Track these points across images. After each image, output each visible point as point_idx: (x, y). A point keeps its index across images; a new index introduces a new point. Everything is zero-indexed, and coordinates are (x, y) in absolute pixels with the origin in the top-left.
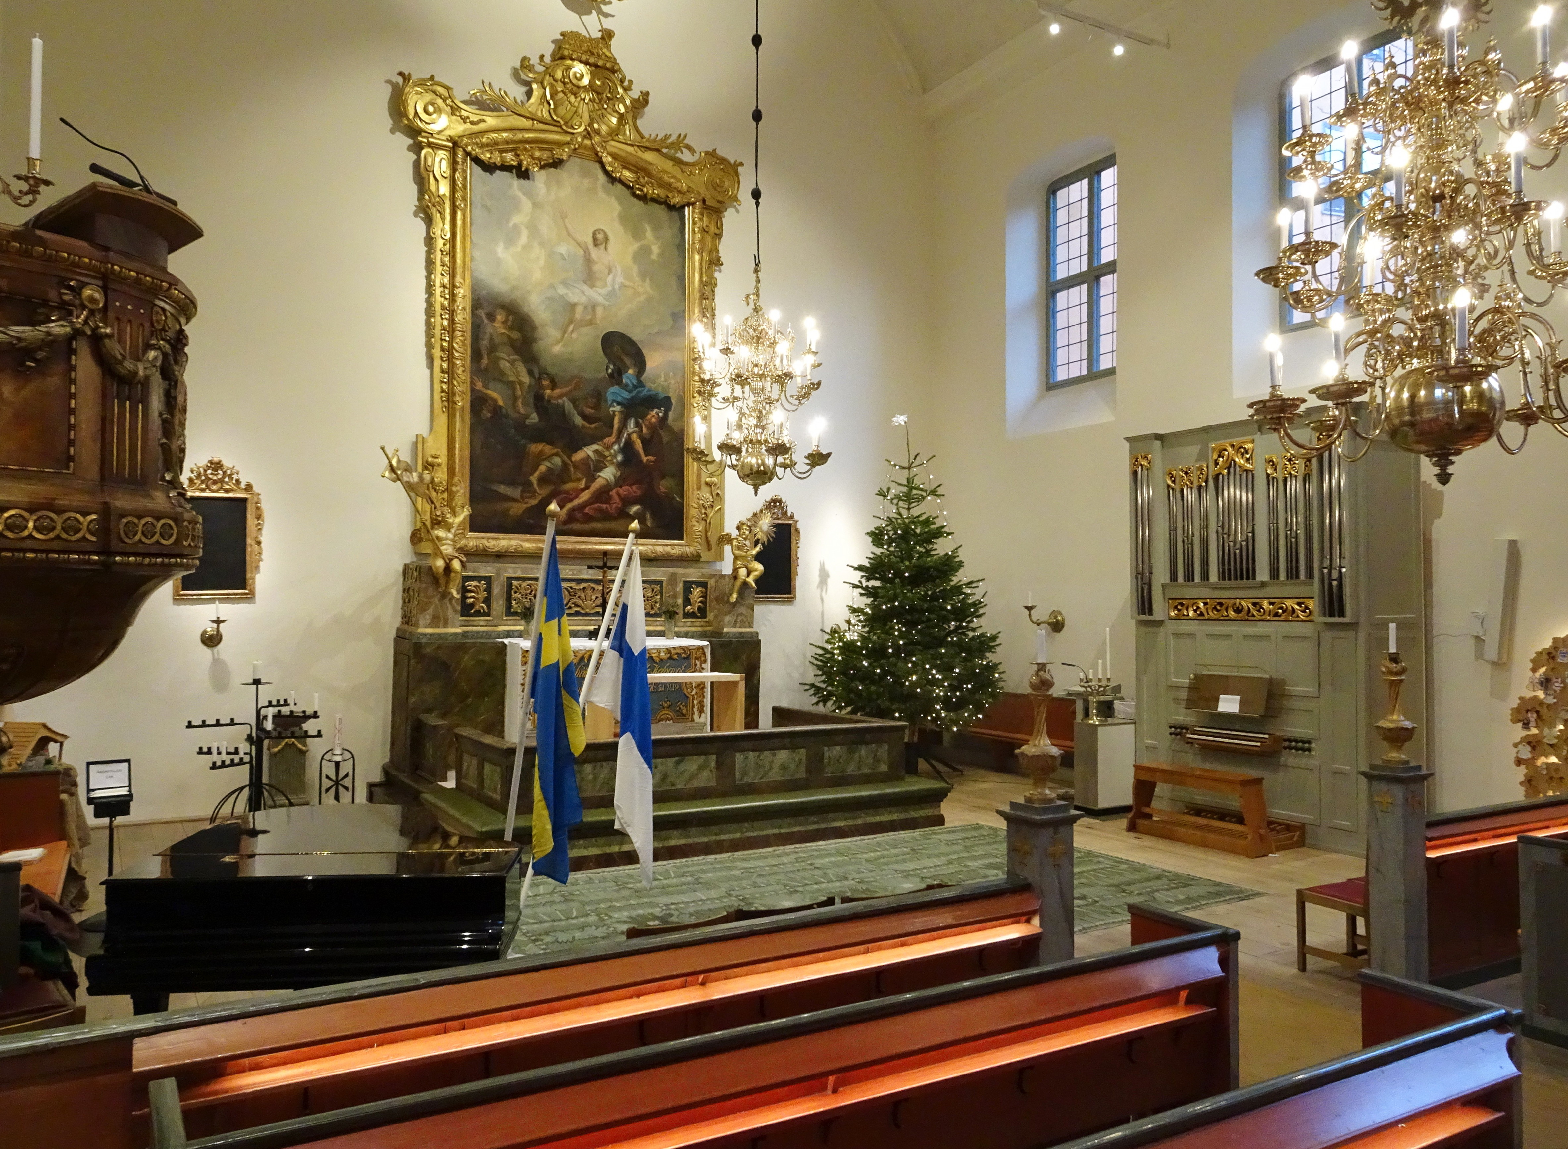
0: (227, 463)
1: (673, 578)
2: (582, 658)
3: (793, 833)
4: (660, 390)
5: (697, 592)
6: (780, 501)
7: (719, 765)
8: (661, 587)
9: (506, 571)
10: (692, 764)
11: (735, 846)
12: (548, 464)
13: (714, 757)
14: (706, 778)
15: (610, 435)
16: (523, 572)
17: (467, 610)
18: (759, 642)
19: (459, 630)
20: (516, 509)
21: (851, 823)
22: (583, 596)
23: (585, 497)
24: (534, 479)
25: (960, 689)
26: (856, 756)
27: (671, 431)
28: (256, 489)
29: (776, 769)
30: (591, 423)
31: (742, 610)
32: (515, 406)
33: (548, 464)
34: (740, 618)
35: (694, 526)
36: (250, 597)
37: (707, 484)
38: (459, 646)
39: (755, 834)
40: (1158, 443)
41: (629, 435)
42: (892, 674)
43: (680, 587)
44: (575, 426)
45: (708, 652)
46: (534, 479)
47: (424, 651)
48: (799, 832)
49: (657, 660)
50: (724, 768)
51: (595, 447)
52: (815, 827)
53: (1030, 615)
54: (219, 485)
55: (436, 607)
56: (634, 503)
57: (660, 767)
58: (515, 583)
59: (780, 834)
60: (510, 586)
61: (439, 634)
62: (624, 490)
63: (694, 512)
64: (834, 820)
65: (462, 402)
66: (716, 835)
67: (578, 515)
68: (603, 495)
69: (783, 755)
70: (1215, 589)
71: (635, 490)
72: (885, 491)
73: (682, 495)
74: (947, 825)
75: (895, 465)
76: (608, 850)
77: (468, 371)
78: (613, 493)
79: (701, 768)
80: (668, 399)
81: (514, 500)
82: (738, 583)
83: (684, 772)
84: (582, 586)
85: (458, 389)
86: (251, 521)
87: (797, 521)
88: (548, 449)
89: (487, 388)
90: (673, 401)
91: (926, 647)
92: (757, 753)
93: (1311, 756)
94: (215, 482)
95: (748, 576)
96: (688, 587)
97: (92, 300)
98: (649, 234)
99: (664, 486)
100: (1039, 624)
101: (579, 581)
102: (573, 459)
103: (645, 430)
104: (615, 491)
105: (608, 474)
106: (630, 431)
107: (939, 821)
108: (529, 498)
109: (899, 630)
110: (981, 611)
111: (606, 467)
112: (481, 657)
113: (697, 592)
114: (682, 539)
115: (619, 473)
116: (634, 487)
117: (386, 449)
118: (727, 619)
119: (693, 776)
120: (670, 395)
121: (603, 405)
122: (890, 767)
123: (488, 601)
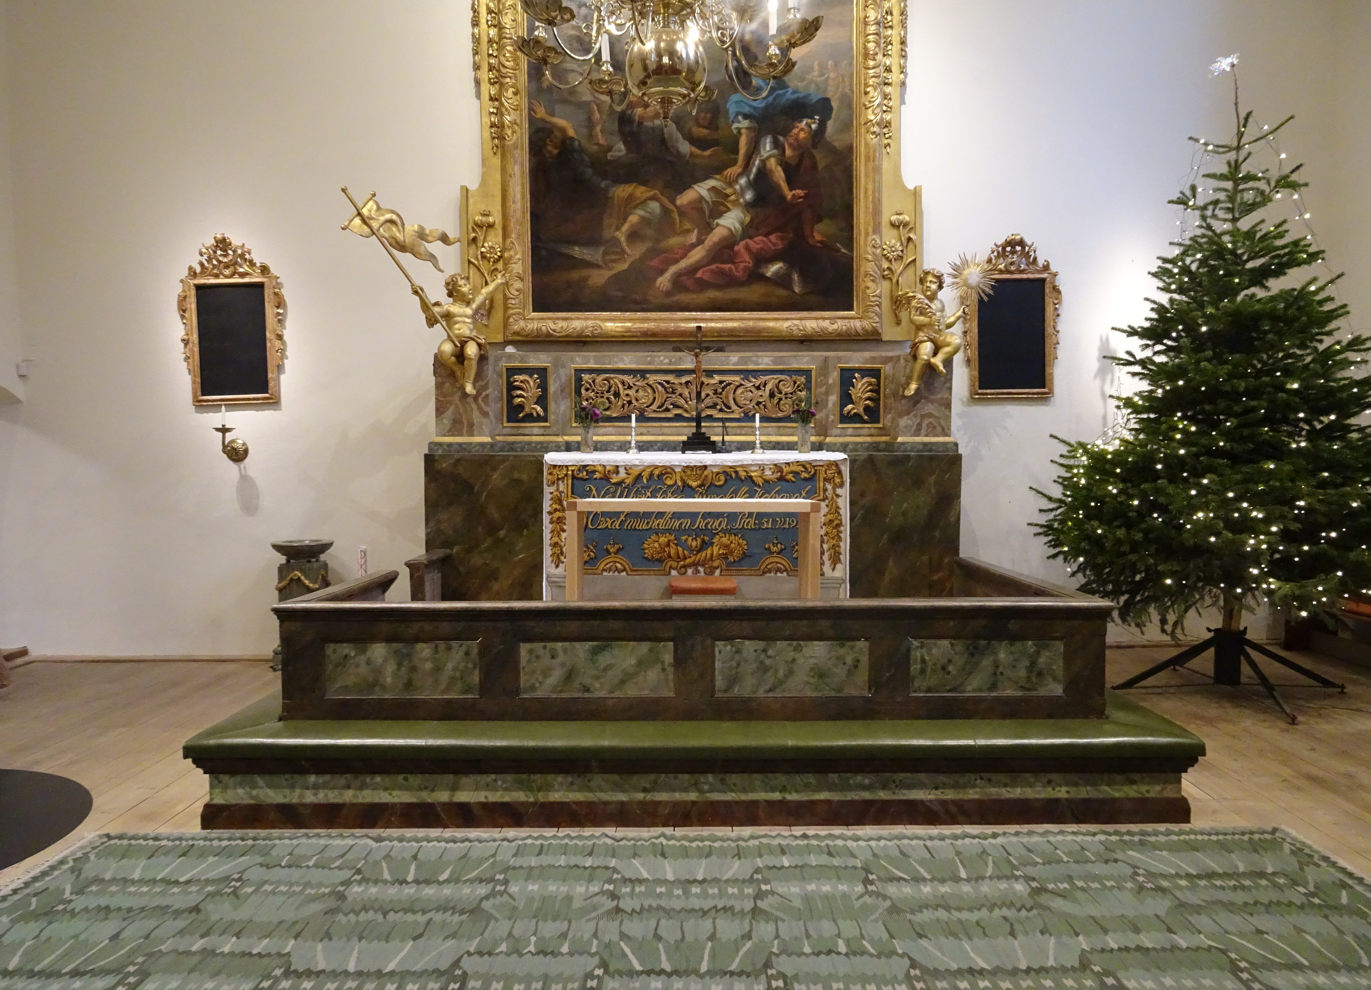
0: (236, 241)
1: (825, 367)
2: (639, 477)
3: (813, 802)
4: (812, 89)
5: (861, 387)
6: (1021, 243)
7: (679, 662)
8: (809, 380)
9: (573, 361)
10: (625, 656)
11: (683, 816)
12: (641, 213)
15: (734, 163)
18: (958, 458)
19: (487, 439)
20: (598, 278)
21: (950, 795)
23: (697, 255)
24: (621, 235)
25: (1313, 539)
26: (987, 662)
27: (832, 150)
28: (274, 270)
29: (801, 677)
30: (704, 148)
31: (929, 408)
32: (591, 136)
33: (641, 213)
34: (926, 422)
35: (871, 288)
36: (274, 402)
37: (893, 225)
41: (763, 162)
42: (1163, 510)
43: (834, 377)
44: (679, 155)
47: (438, 466)
48: (828, 802)
49: (760, 481)
51: (711, 183)
52: (867, 795)
54: (232, 269)
55: (457, 406)
57: (561, 658)
58: (586, 377)
59: (783, 802)
60: (579, 381)
61: (460, 445)
62: (757, 243)
63: (870, 267)
64: (910, 787)
65: (519, 137)
66: (645, 790)
67: (689, 282)
69: (818, 651)
71: (775, 241)
72: (1188, 193)
73: (849, 242)
74: (1197, 822)
75: (1206, 144)
76: (427, 797)
77: (523, 93)
79: (642, 664)
80: (826, 102)
81: (597, 266)
82: (918, 366)
84: (684, 380)
85: (507, 119)
86: (270, 311)
87: (1055, 275)
88: (641, 191)
89: (553, 115)
90: (834, 104)
91: (1234, 458)
92: (761, 644)
94: (227, 267)
95: (935, 354)
99: (820, 232)
101: (680, 373)
102: (678, 202)
103: (788, 152)
104: (742, 244)
105: (732, 220)
106: (765, 155)
107: (1179, 811)
108: (614, 261)
109: (1185, 431)
111: (729, 210)
112: (516, 475)
113: (861, 387)
114: (850, 308)
115: (748, 219)
116: (773, 237)
117: (350, 191)
118: (904, 422)
120: (829, 95)
121: (722, 121)
123: (542, 400)
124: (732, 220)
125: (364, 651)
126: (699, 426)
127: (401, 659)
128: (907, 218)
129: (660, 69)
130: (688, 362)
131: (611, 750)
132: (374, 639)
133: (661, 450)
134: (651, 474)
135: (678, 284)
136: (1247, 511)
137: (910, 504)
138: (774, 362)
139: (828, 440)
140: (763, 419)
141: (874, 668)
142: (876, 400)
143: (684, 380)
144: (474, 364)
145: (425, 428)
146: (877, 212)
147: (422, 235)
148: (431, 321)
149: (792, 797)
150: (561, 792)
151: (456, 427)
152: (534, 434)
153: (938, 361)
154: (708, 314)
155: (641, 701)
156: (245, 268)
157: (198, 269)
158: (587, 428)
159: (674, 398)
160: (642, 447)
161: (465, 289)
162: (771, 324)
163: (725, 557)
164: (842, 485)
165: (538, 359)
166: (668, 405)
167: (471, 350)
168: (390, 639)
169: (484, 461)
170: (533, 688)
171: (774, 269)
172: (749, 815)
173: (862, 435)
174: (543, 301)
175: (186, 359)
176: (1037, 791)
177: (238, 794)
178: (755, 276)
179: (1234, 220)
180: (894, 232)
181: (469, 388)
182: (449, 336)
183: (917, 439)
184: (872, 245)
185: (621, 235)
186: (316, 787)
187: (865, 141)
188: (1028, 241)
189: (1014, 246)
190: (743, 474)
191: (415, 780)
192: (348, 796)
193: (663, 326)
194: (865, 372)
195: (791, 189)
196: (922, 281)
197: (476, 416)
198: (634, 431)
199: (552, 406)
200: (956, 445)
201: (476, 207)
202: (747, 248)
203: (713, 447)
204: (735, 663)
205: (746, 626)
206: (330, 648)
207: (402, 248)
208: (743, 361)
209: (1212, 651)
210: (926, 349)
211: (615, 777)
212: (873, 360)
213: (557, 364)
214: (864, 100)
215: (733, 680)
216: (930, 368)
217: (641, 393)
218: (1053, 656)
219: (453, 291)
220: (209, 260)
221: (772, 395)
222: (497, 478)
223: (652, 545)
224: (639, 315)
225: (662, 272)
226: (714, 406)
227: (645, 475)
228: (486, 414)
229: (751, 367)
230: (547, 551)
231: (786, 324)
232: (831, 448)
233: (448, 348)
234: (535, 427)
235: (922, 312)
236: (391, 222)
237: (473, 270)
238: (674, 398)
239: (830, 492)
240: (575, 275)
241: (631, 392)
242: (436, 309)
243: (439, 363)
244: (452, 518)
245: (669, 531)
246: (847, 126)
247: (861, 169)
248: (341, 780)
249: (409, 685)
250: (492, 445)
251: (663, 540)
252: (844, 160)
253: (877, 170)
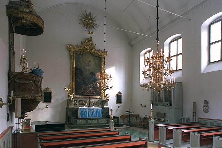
5: (101, 102)
10: (94, 120)
14: (96, 122)
17: (75, 104)
20: (80, 93)
38: (73, 108)
43: (99, 101)
46: (82, 89)
62: (93, 90)
68: (90, 91)
79: (95, 121)
98: (96, 61)
105: (91, 88)
130: (89, 100)
132: (80, 120)
135: (87, 94)
171: (94, 93)
209: (220, 43)
215: (100, 122)
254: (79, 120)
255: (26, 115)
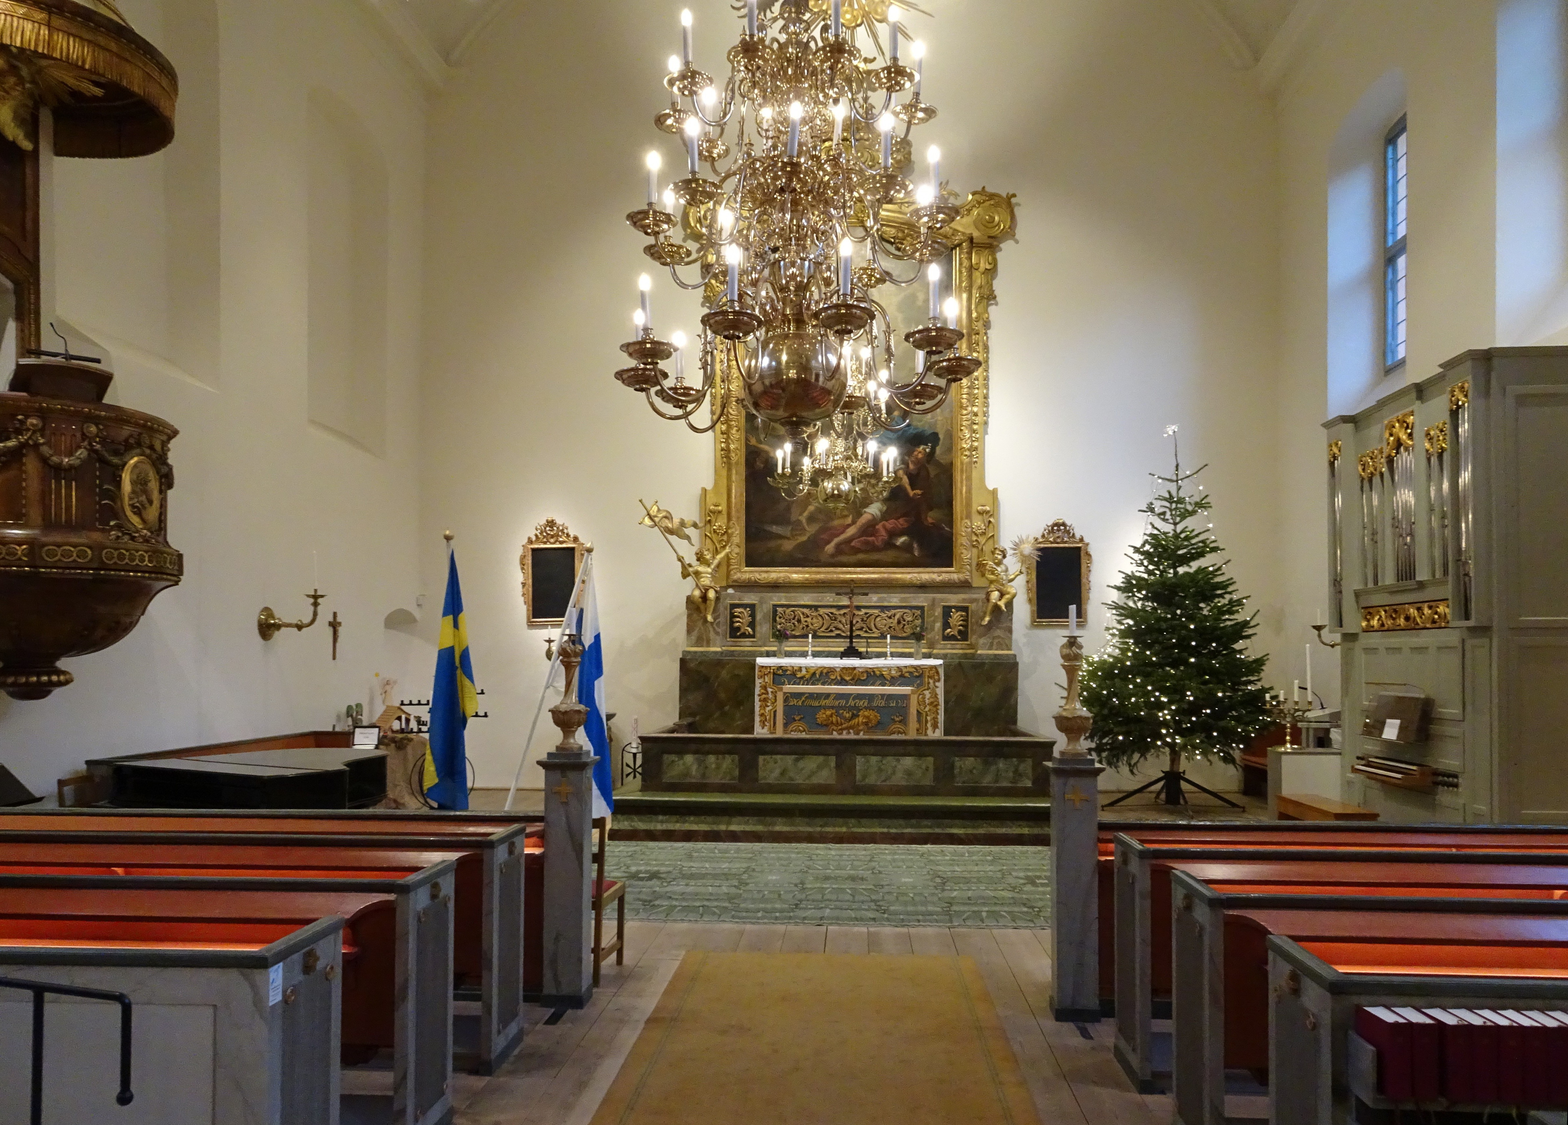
0: (559, 521)
1: (933, 603)
2: (814, 674)
6: (1064, 524)
7: (838, 766)
10: (811, 763)
11: (840, 839)
13: (834, 758)
16: (787, 599)
17: (735, 632)
19: (719, 649)
20: (788, 546)
21: (970, 831)
22: (844, 620)
23: (851, 531)
24: (803, 519)
25: (1198, 714)
26: (993, 768)
27: (938, 464)
29: (899, 774)
31: (998, 632)
34: (996, 641)
35: (964, 553)
39: (862, 830)
40: (1350, 426)
43: (938, 612)
45: (941, 671)
49: (888, 678)
50: (844, 769)
53: (1319, 636)
56: (901, 534)
59: (889, 833)
60: (775, 612)
62: (890, 524)
65: (738, 456)
68: (870, 528)
70: (1392, 593)
71: (902, 523)
73: (950, 523)
76: (715, 828)
78: (879, 527)
79: (820, 767)
83: (802, 769)
84: (842, 612)
85: (732, 447)
87: (1087, 544)
90: (941, 436)
93: (1457, 794)
94: (552, 537)
96: (947, 611)
97: (33, 425)
100: (1333, 646)
101: (839, 607)
103: (911, 466)
105: (874, 509)
110: (1250, 631)
112: (736, 672)
113: (956, 618)
114: (951, 566)
116: (901, 520)
118: (982, 641)
119: (813, 773)
122: (1033, 783)
123: (752, 625)
124: (874, 509)
125: (682, 758)
126: (851, 642)
127: (700, 763)
128: (988, 508)
129: (833, 495)
130: (845, 602)
131: (806, 804)
132: (687, 752)
133: (827, 656)
134: (821, 673)
136: (1159, 697)
137: (984, 691)
138: (902, 600)
139: (935, 651)
140: (892, 638)
141: (936, 769)
142: (966, 626)
143: (842, 612)
144: (713, 603)
145: (679, 640)
146: (969, 504)
147: (683, 524)
148: (685, 575)
149: (893, 831)
150: (780, 827)
151: (699, 642)
152: (746, 646)
153: (1002, 604)
154: (859, 569)
155: (820, 785)
156: (563, 538)
157: (534, 538)
158: (780, 642)
159: (836, 624)
160: (816, 655)
161: (708, 557)
162: (899, 576)
163: (866, 724)
164: (939, 680)
165: (750, 598)
166: (832, 628)
167: (711, 594)
168: (695, 752)
169: (717, 662)
170: (765, 778)
172: (872, 839)
173: (956, 649)
174: (751, 560)
175: (524, 595)
176: (1015, 830)
177: (625, 825)
178: (889, 545)
179: (1175, 524)
180: (980, 517)
181: (710, 618)
182: (697, 585)
183: (991, 652)
184: (965, 528)
185: (803, 519)
186: (662, 822)
187: (961, 460)
188: (1068, 523)
189: (1059, 527)
190: (878, 673)
191: (709, 819)
192: (678, 826)
193: (829, 576)
194: (959, 609)
195: (913, 489)
196: (993, 553)
197: (712, 635)
198: (810, 644)
199: (758, 628)
200: (1015, 656)
201: (711, 499)
202: (884, 526)
203: (860, 656)
204: (866, 767)
205: (872, 749)
206: (665, 756)
207: (671, 532)
208: (880, 600)
210: (995, 595)
211: (806, 820)
212: (964, 600)
213: (761, 602)
214: (960, 434)
215: (864, 777)
216: (996, 607)
217: (815, 620)
218: (1027, 766)
219: (700, 558)
220: (541, 533)
221: (899, 622)
222: (724, 674)
223: (822, 716)
224: (814, 569)
225: (829, 542)
226: (861, 629)
227: (818, 673)
228: (717, 633)
229: (886, 604)
230: (757, 719)
231: (909, 576)
232: (936, 657)
233: (697, 593)
234: (747, 641)
235: (993, 573)
236: (666, 517)
237: (708, 541)
238: (836, 624)
239: (932, 685)
240: (772, 544)
241: (809, 620)
242: (691, 569)
243: (690, 600)
244: (695, 698)
245: (833, 707)
246: (950, 449)
247: (958, 477)
248: (674, 818)
249: (704, 776)
250: (722, 653)
251: (828, 713)
252: (947, 472)
253: (969, 479)
254: (681, 753)
255: (59, 672)
